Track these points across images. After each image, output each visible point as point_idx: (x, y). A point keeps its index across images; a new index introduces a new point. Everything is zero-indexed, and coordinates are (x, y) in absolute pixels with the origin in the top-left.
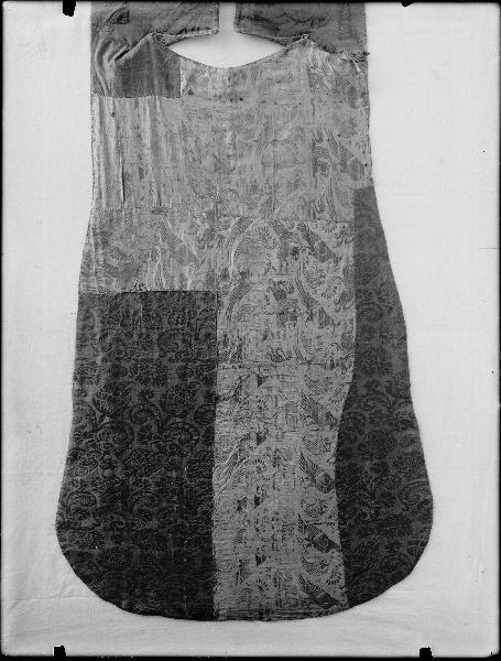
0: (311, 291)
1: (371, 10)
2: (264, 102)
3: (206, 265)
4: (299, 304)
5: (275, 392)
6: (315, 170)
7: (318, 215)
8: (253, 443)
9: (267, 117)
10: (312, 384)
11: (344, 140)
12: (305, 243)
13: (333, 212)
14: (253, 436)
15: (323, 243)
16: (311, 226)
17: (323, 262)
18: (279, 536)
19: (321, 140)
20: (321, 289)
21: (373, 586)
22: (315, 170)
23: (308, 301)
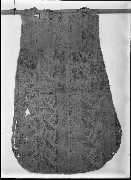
0: (82, 71)
1: (130, 14)
2: (70, 21)
3: (54, 64)
4: (79, 74)
5: (73, 99)
6: (82, 39)
7: (83, 50)
8: (68, 115)
9: (70, 25)
10: (83, 96)
11: (90, 30)
12: (44, 107)
13: (87, 50)
14: (68, 113)
15: (85, 58)
16: (81, 53)
17: (85, 62)
18: (77, 143)
19: (84, 31)
20: (85, 70)
21: (107, 85)
22: (82, 39)
23: (81, 73)
